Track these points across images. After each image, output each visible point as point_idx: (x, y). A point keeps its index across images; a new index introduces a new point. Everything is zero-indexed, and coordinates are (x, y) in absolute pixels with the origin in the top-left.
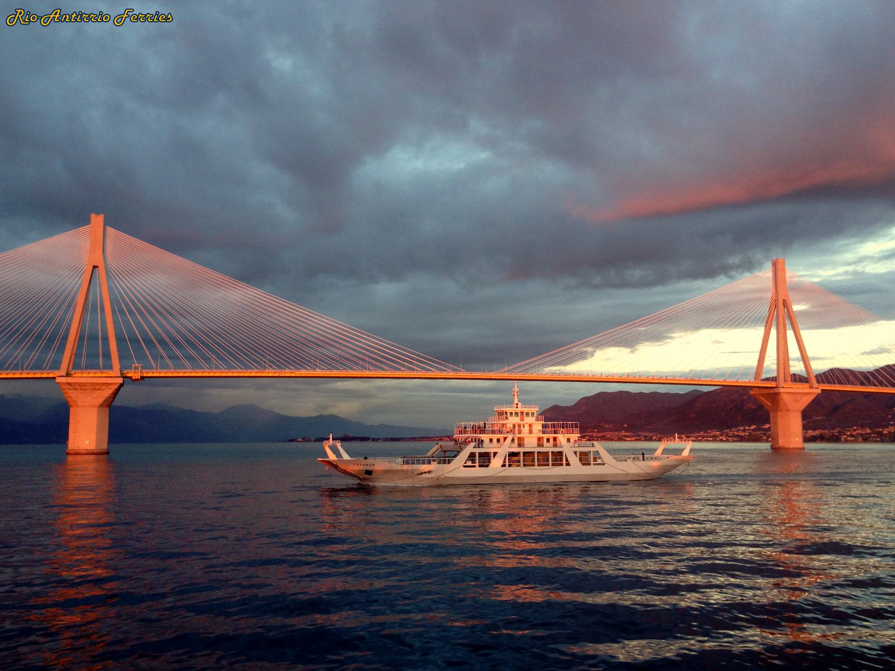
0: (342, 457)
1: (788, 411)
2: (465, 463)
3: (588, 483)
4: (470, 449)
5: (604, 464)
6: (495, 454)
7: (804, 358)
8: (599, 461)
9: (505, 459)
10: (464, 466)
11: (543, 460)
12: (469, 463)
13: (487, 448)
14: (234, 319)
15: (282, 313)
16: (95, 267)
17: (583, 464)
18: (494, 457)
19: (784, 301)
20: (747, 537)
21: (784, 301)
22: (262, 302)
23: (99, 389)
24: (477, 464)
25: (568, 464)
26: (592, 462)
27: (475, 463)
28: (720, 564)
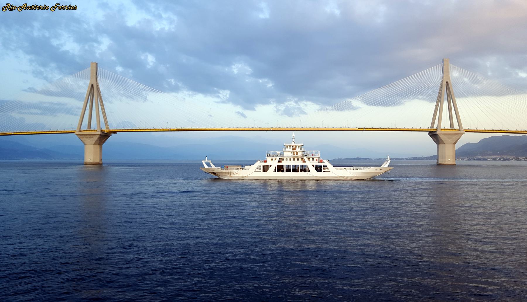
0: (212, 167)
1: (445, 144)
3: (319, 182)
4: (258, 164)
5: (329, 171)
6: (270, 166)
7: (106, 124)
12: (258, 170)
19: (447, 82)
23: (92, 137)
25: (309, 171)
26: (323, 170)
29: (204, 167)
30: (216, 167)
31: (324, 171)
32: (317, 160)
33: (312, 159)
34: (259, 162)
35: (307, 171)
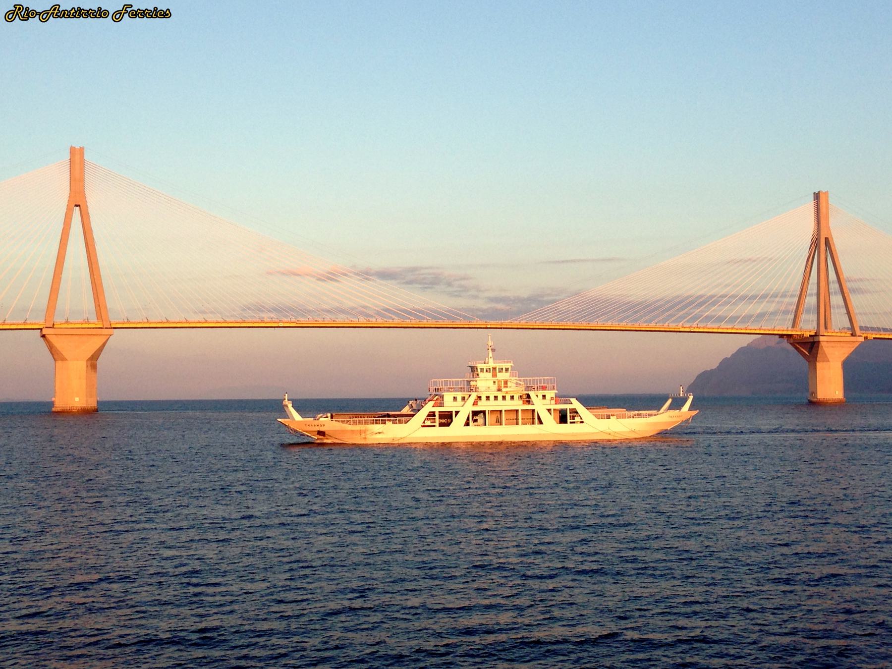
2: (424, 422)
3: (562, 447)
4: (429, 408)
5: (582, 422)
6: (457, 413)
7: (792, 296)
10: (423, 426)
11: (514, 417)
12: (428, 423)
13: (449, 405)
16: (817, 196)
18: (456, 416)
19: (827, 239)
20: (335, 521)
21: (827, 239)
24: (437, 424)
25: (541, 422)
26: (569, 420)
27: (435, 422)
29: (294, 419)
30: (303, 418)
31: (571, 423)
32: (552, 398)
33: (495, 397)
34: (432, 403)
35: (504, 422)
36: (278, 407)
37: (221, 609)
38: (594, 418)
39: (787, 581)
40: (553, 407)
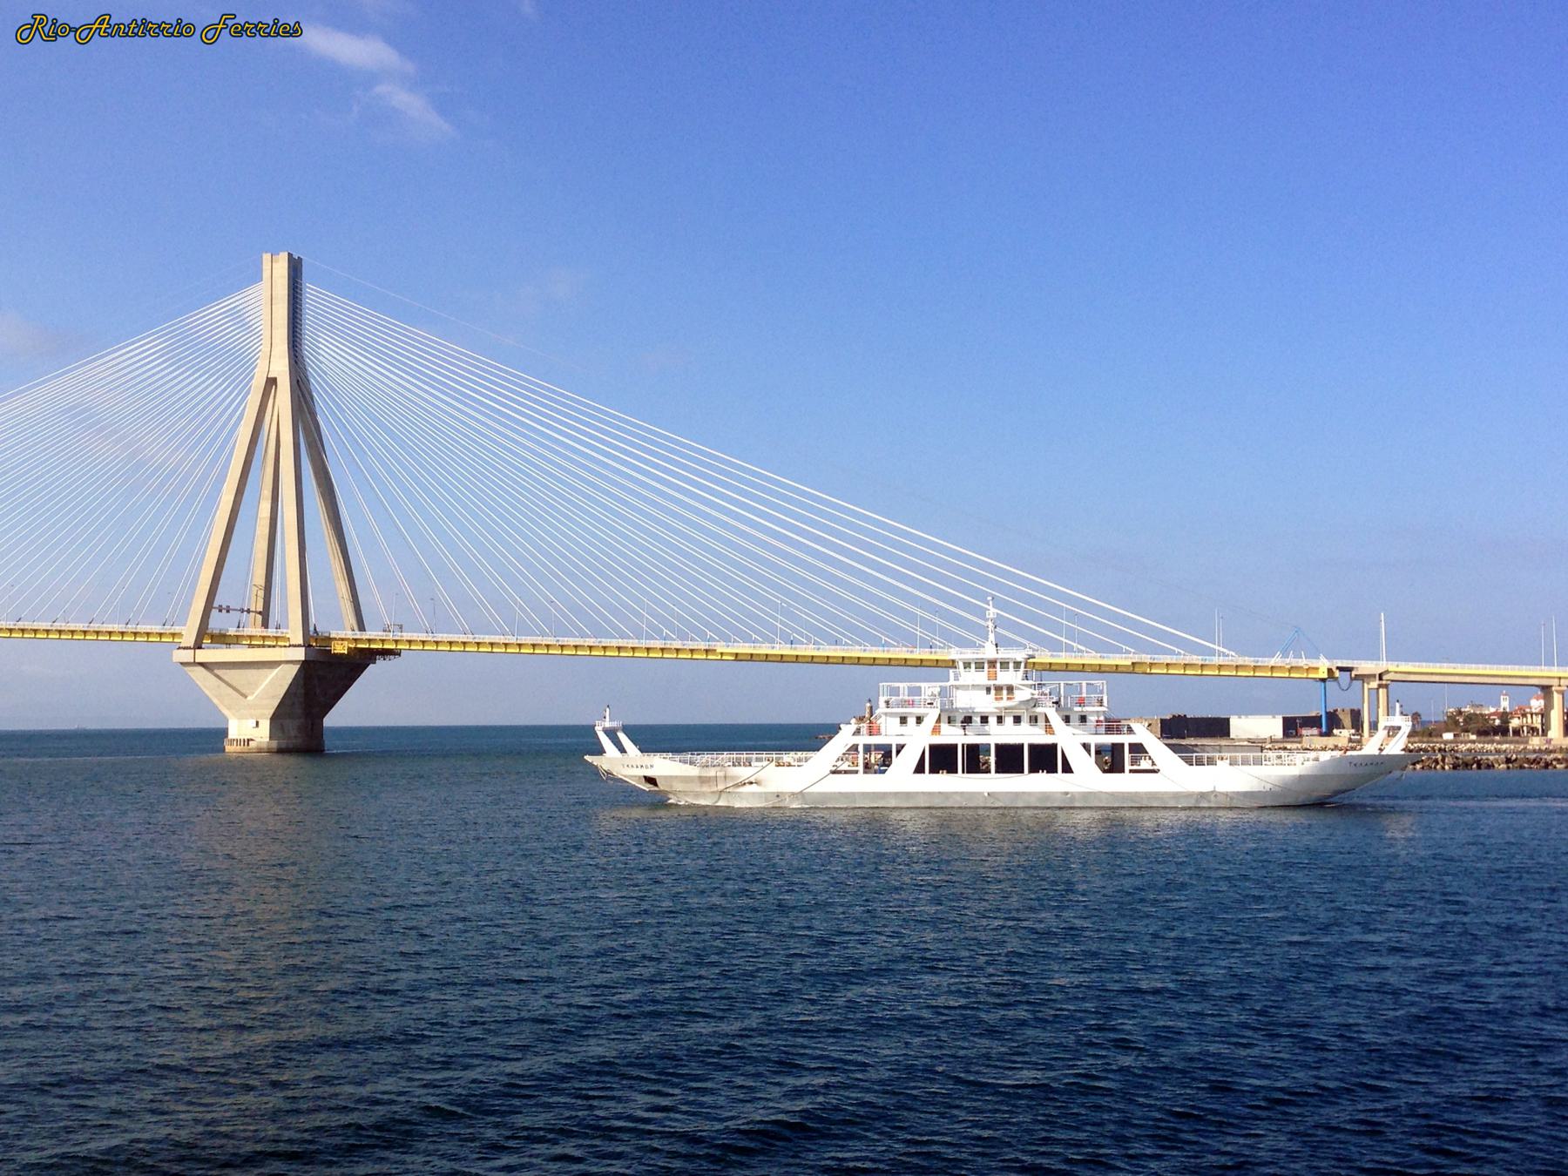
8: (1145, 764)
9: (924, 753)
10: (834, 772)
13: (890, 731)
14: (171, 365)
15: (416, 404)
17: (1105, 771)
22: (719, 547)
25: (1067, 769)
26: (1128, 767)
28: (1407, 660)
31: (1131, 771)
36: (583, 741)
37: (710, 994)
38: (1066, 790)
39: (138, 1030)
40: (1094, 740)
